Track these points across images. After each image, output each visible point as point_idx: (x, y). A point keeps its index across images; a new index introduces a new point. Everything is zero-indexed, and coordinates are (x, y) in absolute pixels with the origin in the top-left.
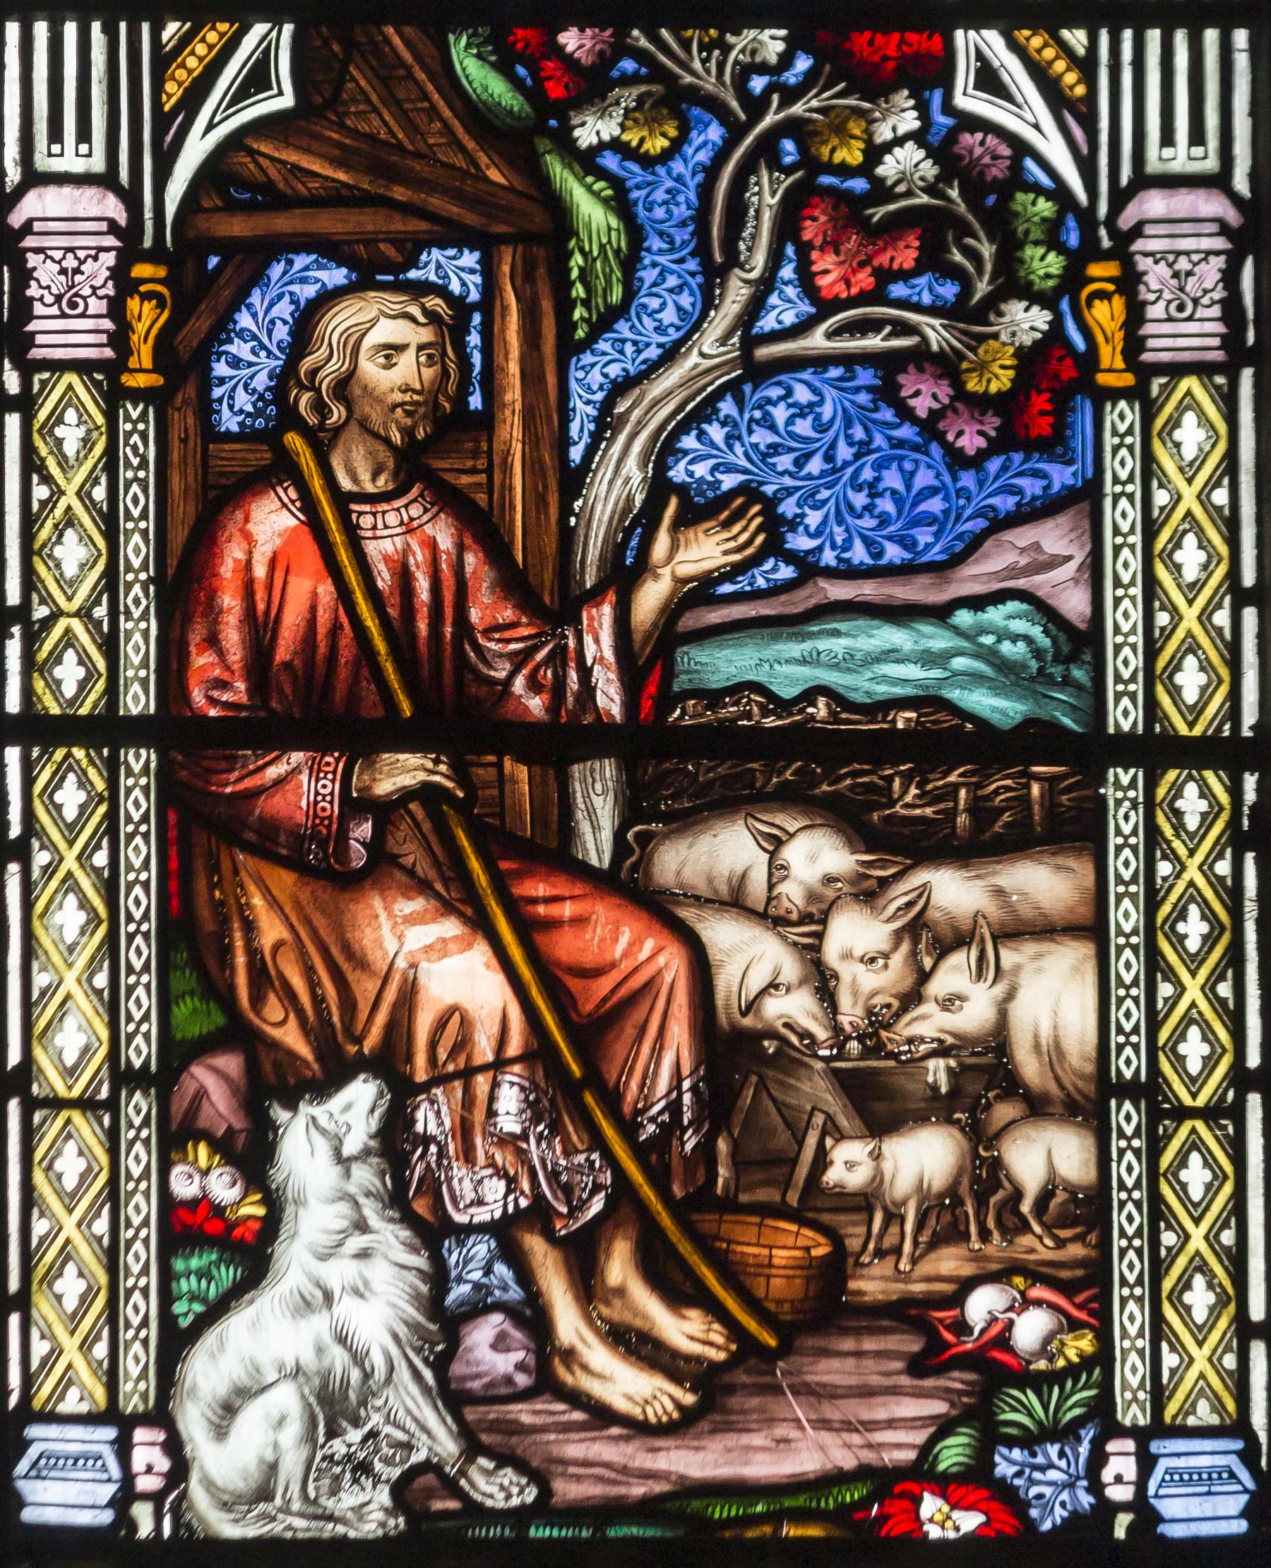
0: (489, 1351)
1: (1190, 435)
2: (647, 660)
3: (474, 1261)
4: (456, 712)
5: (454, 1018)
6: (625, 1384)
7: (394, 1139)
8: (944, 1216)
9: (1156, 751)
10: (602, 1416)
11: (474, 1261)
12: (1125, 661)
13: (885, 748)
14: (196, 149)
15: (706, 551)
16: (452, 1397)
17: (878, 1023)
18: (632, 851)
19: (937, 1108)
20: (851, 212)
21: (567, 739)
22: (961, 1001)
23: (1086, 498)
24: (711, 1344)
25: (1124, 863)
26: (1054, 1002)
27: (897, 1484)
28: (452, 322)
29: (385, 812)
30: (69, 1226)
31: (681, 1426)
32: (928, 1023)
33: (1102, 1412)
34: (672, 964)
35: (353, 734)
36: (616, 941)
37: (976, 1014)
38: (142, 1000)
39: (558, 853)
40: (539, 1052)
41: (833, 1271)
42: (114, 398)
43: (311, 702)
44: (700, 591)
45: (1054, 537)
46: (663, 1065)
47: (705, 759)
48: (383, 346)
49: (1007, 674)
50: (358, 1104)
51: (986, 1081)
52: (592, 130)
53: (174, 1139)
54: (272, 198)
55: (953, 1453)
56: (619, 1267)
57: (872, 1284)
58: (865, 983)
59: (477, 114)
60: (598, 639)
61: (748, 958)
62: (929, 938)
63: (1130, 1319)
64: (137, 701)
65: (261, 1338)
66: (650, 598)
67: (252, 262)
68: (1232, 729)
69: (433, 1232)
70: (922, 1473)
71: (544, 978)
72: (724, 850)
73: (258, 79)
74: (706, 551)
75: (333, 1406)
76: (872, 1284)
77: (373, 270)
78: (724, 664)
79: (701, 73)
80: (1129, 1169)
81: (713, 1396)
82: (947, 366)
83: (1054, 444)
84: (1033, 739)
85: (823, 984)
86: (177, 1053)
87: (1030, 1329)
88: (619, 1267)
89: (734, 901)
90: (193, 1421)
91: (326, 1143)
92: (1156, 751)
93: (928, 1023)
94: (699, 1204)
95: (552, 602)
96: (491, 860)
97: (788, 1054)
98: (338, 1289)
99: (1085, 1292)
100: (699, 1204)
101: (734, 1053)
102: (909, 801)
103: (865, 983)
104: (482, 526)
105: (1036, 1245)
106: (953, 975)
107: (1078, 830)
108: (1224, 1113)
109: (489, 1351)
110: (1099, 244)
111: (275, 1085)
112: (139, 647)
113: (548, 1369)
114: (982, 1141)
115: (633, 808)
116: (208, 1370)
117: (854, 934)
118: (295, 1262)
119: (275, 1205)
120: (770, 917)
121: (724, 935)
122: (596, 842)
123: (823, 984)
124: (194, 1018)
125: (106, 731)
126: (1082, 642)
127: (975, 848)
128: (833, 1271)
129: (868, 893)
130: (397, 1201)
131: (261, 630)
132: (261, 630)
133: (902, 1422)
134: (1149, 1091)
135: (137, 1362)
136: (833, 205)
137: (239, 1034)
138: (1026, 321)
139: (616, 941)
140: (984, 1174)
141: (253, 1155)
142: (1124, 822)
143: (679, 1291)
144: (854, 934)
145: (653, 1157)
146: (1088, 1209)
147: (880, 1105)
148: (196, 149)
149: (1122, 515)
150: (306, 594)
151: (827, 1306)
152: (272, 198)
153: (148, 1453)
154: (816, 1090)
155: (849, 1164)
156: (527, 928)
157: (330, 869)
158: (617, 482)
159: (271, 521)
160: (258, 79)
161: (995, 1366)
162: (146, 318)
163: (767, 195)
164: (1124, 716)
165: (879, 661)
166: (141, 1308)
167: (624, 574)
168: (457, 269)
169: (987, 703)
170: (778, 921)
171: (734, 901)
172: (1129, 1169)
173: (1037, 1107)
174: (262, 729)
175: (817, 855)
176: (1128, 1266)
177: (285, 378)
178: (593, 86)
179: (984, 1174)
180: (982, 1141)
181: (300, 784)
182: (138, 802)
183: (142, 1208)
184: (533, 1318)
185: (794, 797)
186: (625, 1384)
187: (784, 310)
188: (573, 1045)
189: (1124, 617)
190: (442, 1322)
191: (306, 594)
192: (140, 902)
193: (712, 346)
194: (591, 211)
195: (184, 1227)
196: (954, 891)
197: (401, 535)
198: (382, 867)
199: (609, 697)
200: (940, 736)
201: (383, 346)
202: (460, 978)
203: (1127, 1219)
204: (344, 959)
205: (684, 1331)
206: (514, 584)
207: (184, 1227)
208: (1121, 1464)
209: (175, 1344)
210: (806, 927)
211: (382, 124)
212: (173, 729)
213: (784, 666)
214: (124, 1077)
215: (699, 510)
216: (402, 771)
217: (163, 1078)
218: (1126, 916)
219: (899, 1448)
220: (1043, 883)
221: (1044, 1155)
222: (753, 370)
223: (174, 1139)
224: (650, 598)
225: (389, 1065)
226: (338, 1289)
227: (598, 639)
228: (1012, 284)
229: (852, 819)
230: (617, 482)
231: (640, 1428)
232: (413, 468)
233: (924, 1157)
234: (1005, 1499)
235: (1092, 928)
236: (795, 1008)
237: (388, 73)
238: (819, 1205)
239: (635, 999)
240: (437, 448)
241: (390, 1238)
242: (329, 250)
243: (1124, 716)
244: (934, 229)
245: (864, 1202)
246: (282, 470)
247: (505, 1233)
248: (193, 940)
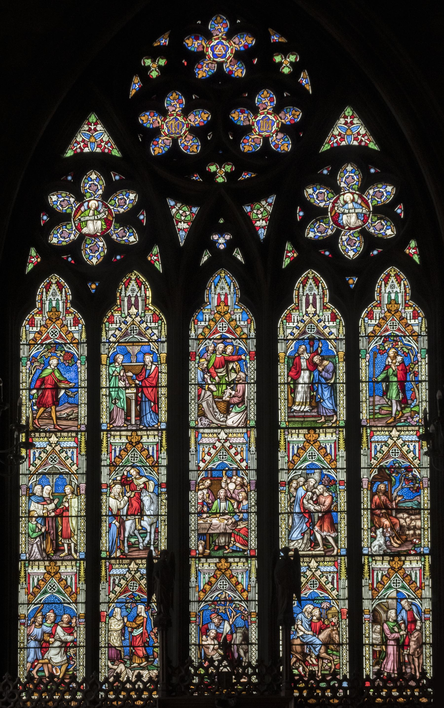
0: (388, 543)
1: (426, 491)
2: (396, 504)
3: (387, 538)
4: (386, 508)
5: (386, 525)
6: (395, 545)
7: (383, 532)
8: (413, 535)
9: (424, 509)
10: (394, 547)
11: (387, 538)
12: (422, 504)
13: (409, 509)
14: (372, 476)
15: (400, 498)
16: (386, 546)
17: (409, 525)
18: (396, 515)
19: (412, 529)
20: (407, 479)
21: (392, 509)
22: (413, 523)
23: (420, 495)
24: (424, 505)
25: (422, 515)
26: (418, 523)
27: (410, 550)
28: (386, 486)
29: (382, 513)
30: (366, 537)
31: (398, 547)
32: (412, 525)
33: (421, 547)
34: (398, 521)
35: (380, 509)
36: (395, 520)
37: (414, 524)
38: (369, 524)
39: (391, 515)
40: (391, 527)
41: (406, 539)
42: (368, 490)
43: (379, 507)
44: (399, 501)
45: (418, 497)
46: (398, 527)
47: (399, 510)
48: (382, 487)
49: (416, 505)
50: (381, 530)
51: (415, 528)
52: (393, 475)
53: (371, 532)
54: (376, 479)
55: (413, 548)
56: (395, 539)
57: (409, 539)
58: (408, 522)
59: (387, 474)
60: (394, 504)
61: (402, 521)
62: (412, 520)
63: (423, 541)
64: (369, 507)
65: (376, 543)
66: (397, 501)
67: (375, 482)
68: (151, 265)
69: (385, 537)
70: (411, 550)
71: (391, 522)
72: (401, 515)
73: (375, 472)
74: (400, 498)
75: (380, 546)
76: (409, 539)
77: (382, 482)
78: (401, 505)
79: (399, 471)
80: (422, 533)
81: (400, 545)
82: (412, 488)
83: (418, 492)
84: (416, 509)
85: (406, 522)
86: (371, 527)
87: (417, 541)
88: (395, 539)
89: (401, 518)
90: (372, 548)
91: (379, 532)
92: (424, 509)
93: (412, 525)
94: (400, 535)
95: (391, 501)
96: (388, 516)
97: (404, 526)
98: (380, 540)
99: (420, 539)
100: (400, 535)
101: (401, 526)
102: (411, 512)
103: (408, 522)
104: (388, 497)
105: (418, 537)
106: (413, 522)
107: (419, 514)
108: (428, 529)
109: (388, 543)
110: (421, 481)
111: (377, 529)
112: (369, 504)
113: (391, 544)
114: (415, 531)
115: (396, 513)
116: (373, 545)
117: (408, 520)
118: (378, 539)
119: (377, 535)
120: (403, 519)
121: (401, 520)
122: (394, 515)
123: (406, 522)
124: (372, 525)
125: (367, 509)
126: (420, 503)
127: (414, 515)
128: (406, 539)
129: (408, 517)
130: (383, 535)
131: (376, 503)
132: (376, 503)
133: (410, 547)
134: (424, 528)
135: (369, 544)
136: (407, 479)
137: (375, 526)
138: (417, 485)
139: (395, 520)
140: (415, 533)
141: (375, 533)
142: (422, 513)
143: (398, 540)
144: (408, 520)
145: (397, 532)
146: (420, 535)
147: (409, 529)
148: (372, 476)
149: (422, 496)
150: (378, 501)
151: (406, 541)
152: (376, 479)
153: (370, 549)
154: (406, 529)
155: (407, 532)
156: (390, 520)
157: (379, 516)
158: (395, 494)
159: (376, 497)
160: (375, 472)
161: (415, 544)
162: (369, 486)
163: (403, 478)
164: (422, 507)
165: (409, 504)
166: (369, 541)
167: (395, 500)
168: (386, 483)
169: (415, 507)
170: (404, 519)
171: (401, 518)
172: (422, 533)
173: (418, 529)
174: (376, 509)
175: (406, 515)
176: (422, 538)
177: (377, 489)
178: (393, 472)
179: (415, 533)
180: (415, 531)
181: (378, 512)
182: (369, 513)
183: (369, 536)
184: (390, 541)
185: (405, 512)
186: (395, 545)
187: (404, 485)
188: (393, 526)
189: (422, 502)
190: (385, 542)
191: (378, 501)
192: (369, 518)
193: (400, 487)
194: (393, 479)
195: (372, 537)
196: (413, 517)
197: (383, 498)
198: (382, 516)
199: (394, 507)
200: (412, 509)
201: (382, 487)
202: (386, 522)
203: (422, 535)
204: (380, 521)
205: (398, 542)
206: (389, 500)
207: (372, 537)
208: (422, 549)
209: (371, 543)
210: (405, 519)
211: (382, 475)
212: (371, 509)
213: (404, 505)
214: (368, 528)
215: (400, 496)
216: (383, 511)
217: (370, 529)
218: (422, 518)
219: (410, 548)
220: (418, 517)
221: (418, 532)
222: (402, 488)
223: (371, 532)
224: (397, 501)
225: (383, 527)
226: (380, 540)
227: (394, 504)
228: (416, 483)
229: (408, 513)
230: (395, 494)
231: (396, 547)
232: (384, 494)
233: (411, 532)
234: (416, 551)
235: (420, 519)
236: (404, 524)
237: (382, 471)
238: (406, 535)
239: (396, 524)
240: (385, 493)
241: (383, 537)
242: (379, 482)
243: (422, 507)
244: (412, 480)
245: (409, 534)
246: (377, 494)
247: (389, 537)
248: (372, 521)
